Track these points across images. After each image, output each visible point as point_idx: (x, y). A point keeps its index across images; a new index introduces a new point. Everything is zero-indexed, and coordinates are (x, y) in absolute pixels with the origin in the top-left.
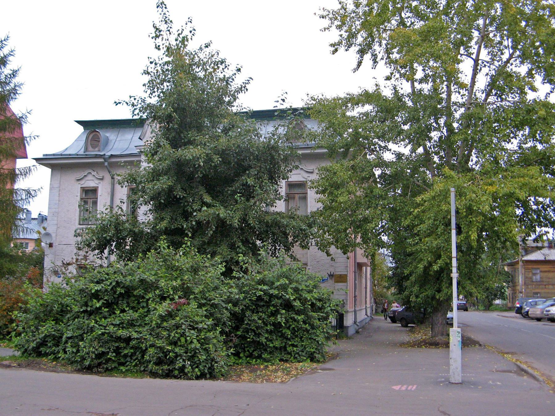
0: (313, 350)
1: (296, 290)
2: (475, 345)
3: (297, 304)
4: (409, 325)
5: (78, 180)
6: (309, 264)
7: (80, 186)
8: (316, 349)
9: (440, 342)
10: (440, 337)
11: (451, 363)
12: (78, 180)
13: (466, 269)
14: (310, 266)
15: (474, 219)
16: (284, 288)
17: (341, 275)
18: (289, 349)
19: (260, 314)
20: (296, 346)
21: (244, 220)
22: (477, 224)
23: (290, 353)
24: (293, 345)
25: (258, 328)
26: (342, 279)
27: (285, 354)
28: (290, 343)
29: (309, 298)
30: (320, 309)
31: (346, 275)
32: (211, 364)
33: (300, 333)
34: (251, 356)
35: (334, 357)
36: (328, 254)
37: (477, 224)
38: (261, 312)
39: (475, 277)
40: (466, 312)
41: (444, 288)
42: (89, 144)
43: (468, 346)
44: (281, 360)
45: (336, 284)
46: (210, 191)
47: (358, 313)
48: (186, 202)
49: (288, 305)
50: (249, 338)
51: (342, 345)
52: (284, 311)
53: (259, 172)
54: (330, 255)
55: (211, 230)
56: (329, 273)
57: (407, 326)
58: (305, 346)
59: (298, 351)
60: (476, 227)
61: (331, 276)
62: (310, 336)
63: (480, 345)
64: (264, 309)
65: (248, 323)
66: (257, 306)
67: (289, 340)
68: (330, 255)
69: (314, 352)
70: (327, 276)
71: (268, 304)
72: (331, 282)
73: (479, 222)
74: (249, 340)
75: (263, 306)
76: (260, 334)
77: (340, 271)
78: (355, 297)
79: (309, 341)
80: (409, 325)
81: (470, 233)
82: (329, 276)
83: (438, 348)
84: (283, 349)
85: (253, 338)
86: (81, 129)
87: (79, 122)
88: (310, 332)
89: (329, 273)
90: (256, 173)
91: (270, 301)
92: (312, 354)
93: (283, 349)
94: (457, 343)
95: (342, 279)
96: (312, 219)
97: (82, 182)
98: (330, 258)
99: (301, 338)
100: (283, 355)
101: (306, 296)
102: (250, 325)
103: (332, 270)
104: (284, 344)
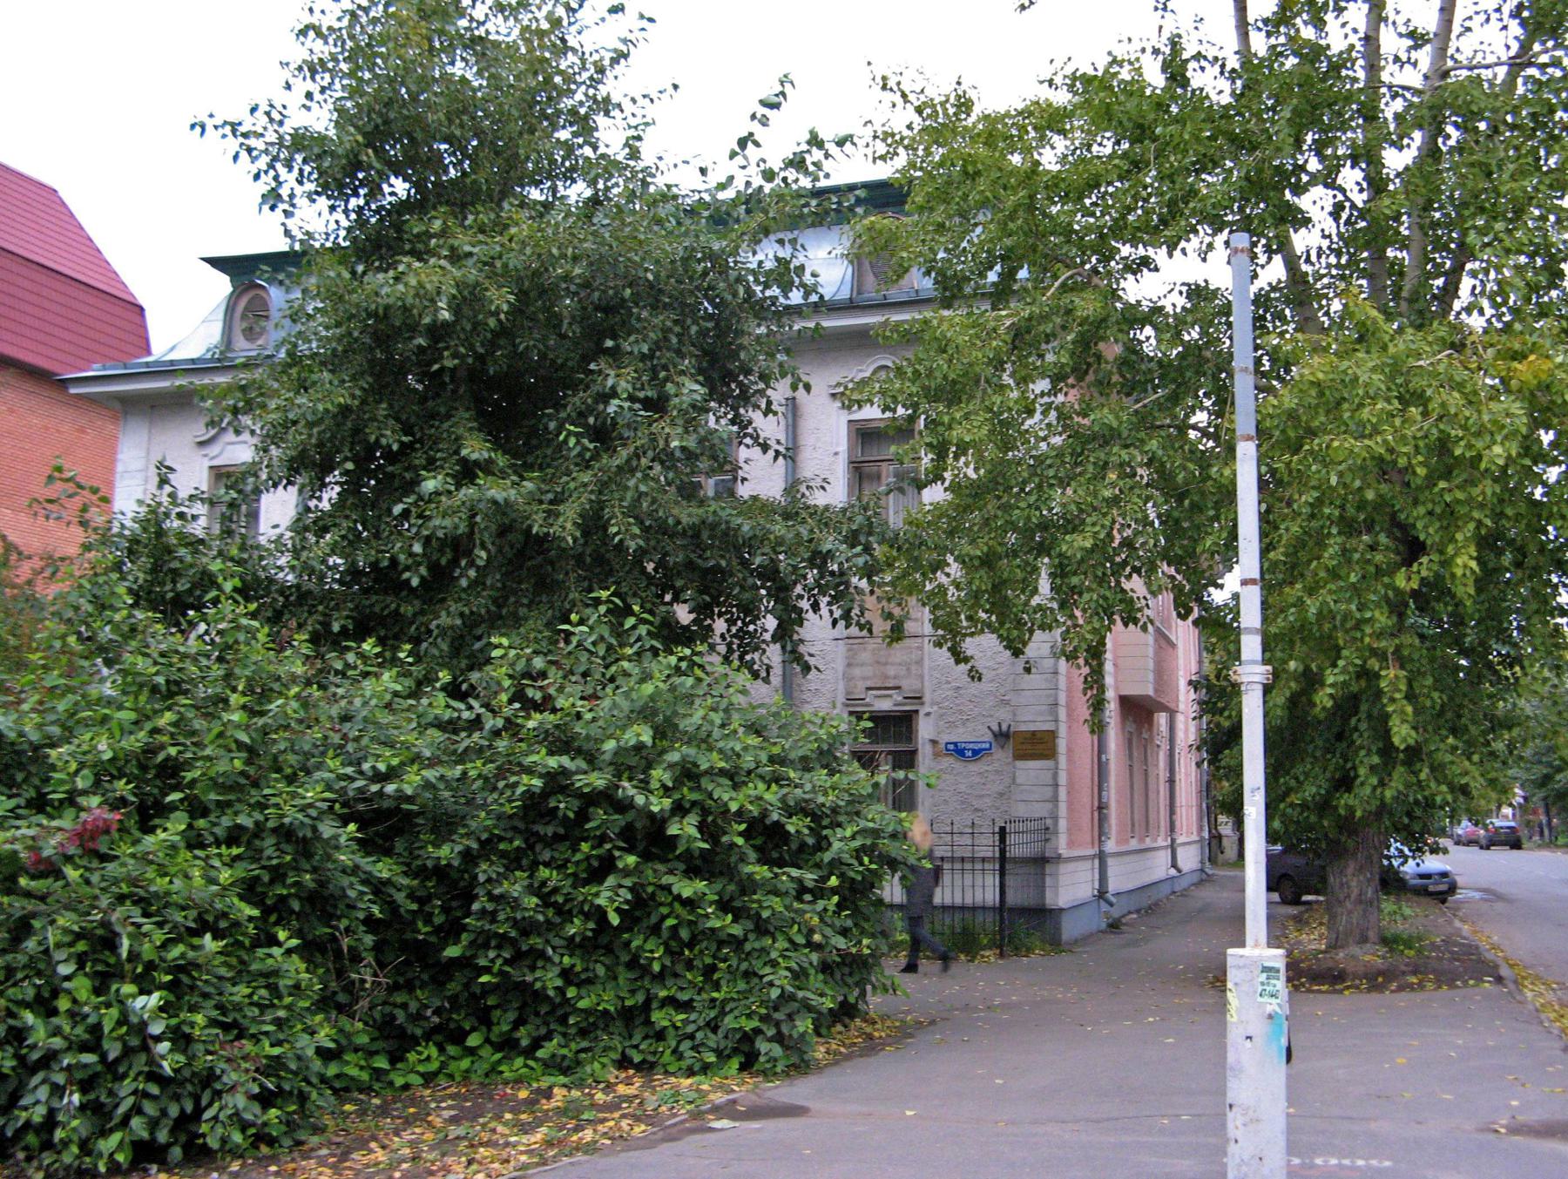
0: (749, 1025)
1: (688, 774)
2: (1480, 980)
3: (686, 829)
4: (1306, 898)
5: (202, 444)
6: (927, 698)
7: (207, 463)
8: (764, 1019)
9: (1350, 969)
10: (1355, 950)
11: (1232, 1132)
12: (202, 444)
13: (1436, 695)
14: (933, 704)
15: (1460, 495)
16: (636, 763)
17: (1120, 742)
18: (659, 1018)
19: (544, 873)
20: (686, 1006)
21: (593, 523)
22: (1476, 514)
23: (660, 1036)
24: (671, 1001)
25: (527, 928)
26: (1038, 745)
27: (635, 1037)
28: (663, 994)
29: (734, 807)
30: (802, 854)
31: (1053, 735)
32: (197, 1099)
33: (706, 948)
34: (508, 1045)
35: (904, 1033)
36: (959, 657)
37: (1476, 514)
38: (546, 865)
39: (1473, 721)
40: (1515, 852)
41: (1362, 771)
42: (238, 326)
43: (1452, 986)
44: (623, 1063)
45: (1019, 764)
46: (496, 426)
47: (1110, 861)
48: (407, 469)
49: (651, 839)
50: (488, 970)
51: (926, 989)
52: (631, 860)
53: (657, 346)
54: (966, 660)
55: (472, 564)
56: (995, 728)
57: (1296, 901)
58: (725, 1001)
59: (690, 1029)
60: (1472, 526)
61: (1002, 736)
62: (744, 966)
63: (1499, 980)
64: (562, 851)
65: (483, 911)
66: (532, 840)
67: (660, 977)
68: (966, 660)
69: (757, 1031)
70: (989, 737)
71: (573, 831)
72: (1001, 756)
73: (1482, 506)
74: (484, 979)
75: (557, 838)
76: (542, 954)
77: (1031, 720)
78: (1100, 808)
79: (742, 985)
80: (1306, 898)
81: (1450, 550)
82: (995, 735)
83: (1341, 992)
84: (633, 1017)
85: (501, 973)
86: (222, 284)
87: (216, 262)
88: (748, 947)
89: (995, 728)
90: (645, 349)
91: (583, 816)
92: (748, 1038)
93: (633, 1017)
94: (1258, 1027)
95: (1038, 745)
96: (859, 519)
97: (214, 450)
98: (963, 667)
99: (709, 971)
100: (636, 1040)
101: (726, 797)
102: (492, 917)
103: (1004, 717)
104: (640, 998)
